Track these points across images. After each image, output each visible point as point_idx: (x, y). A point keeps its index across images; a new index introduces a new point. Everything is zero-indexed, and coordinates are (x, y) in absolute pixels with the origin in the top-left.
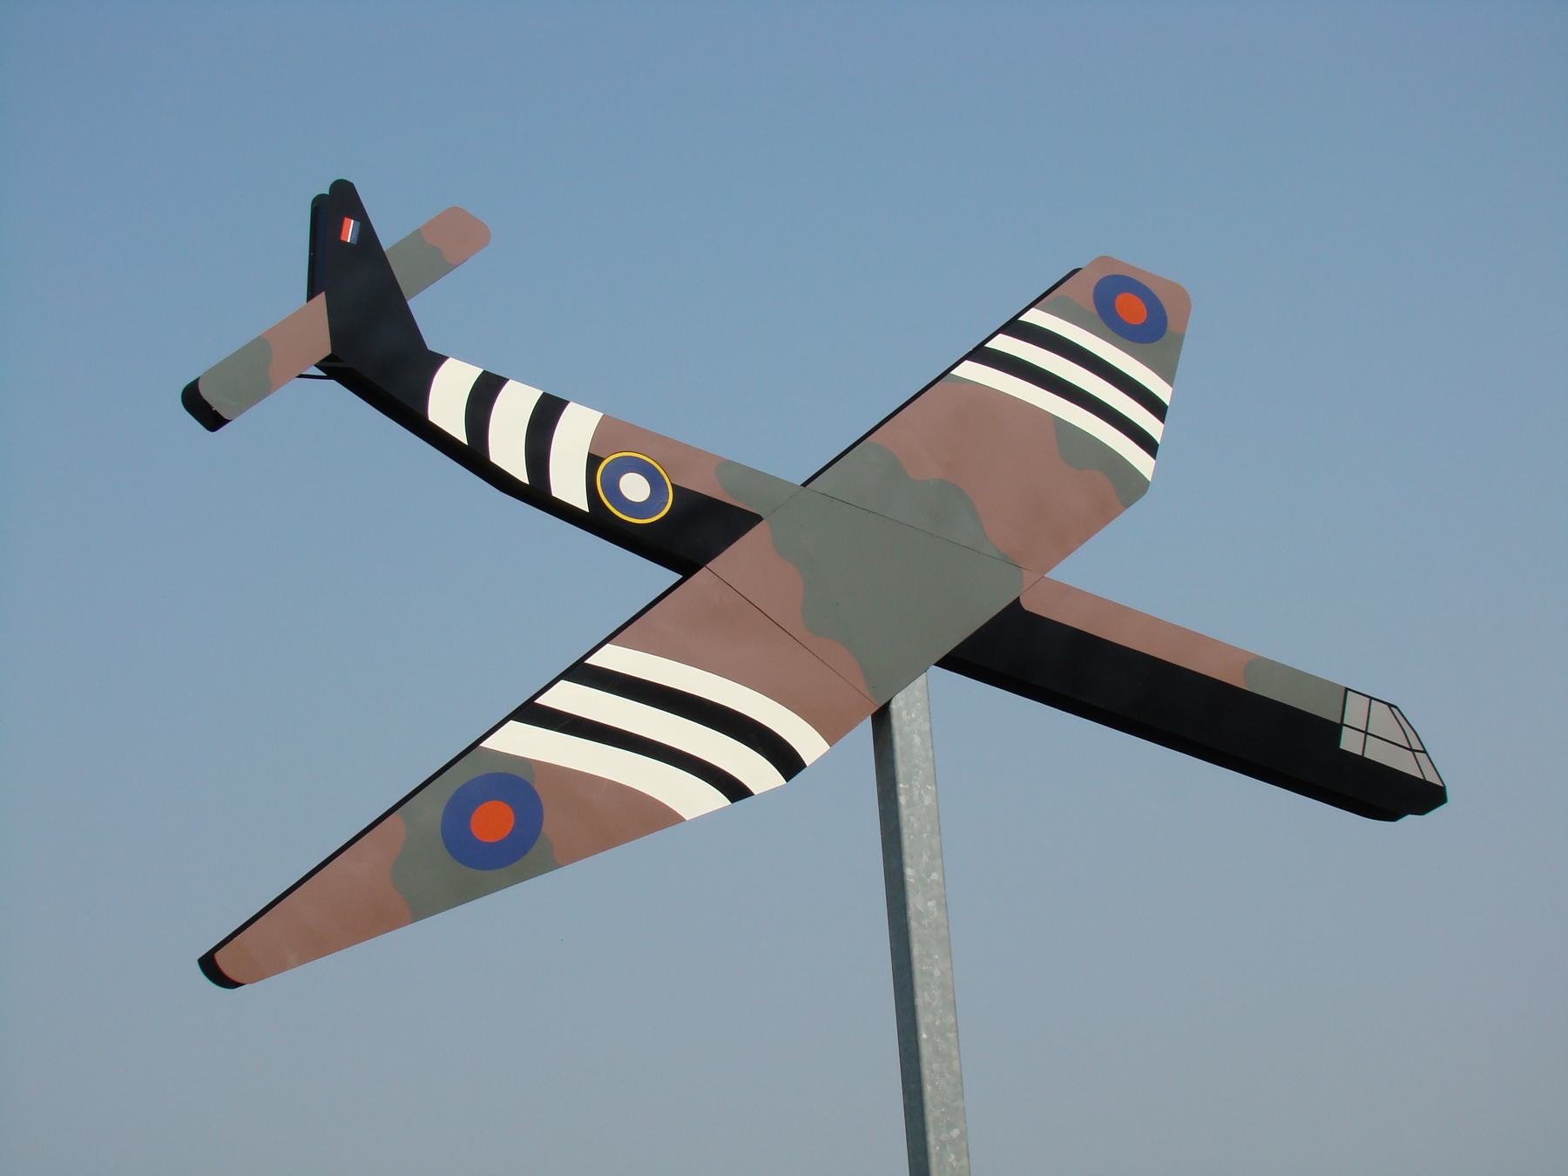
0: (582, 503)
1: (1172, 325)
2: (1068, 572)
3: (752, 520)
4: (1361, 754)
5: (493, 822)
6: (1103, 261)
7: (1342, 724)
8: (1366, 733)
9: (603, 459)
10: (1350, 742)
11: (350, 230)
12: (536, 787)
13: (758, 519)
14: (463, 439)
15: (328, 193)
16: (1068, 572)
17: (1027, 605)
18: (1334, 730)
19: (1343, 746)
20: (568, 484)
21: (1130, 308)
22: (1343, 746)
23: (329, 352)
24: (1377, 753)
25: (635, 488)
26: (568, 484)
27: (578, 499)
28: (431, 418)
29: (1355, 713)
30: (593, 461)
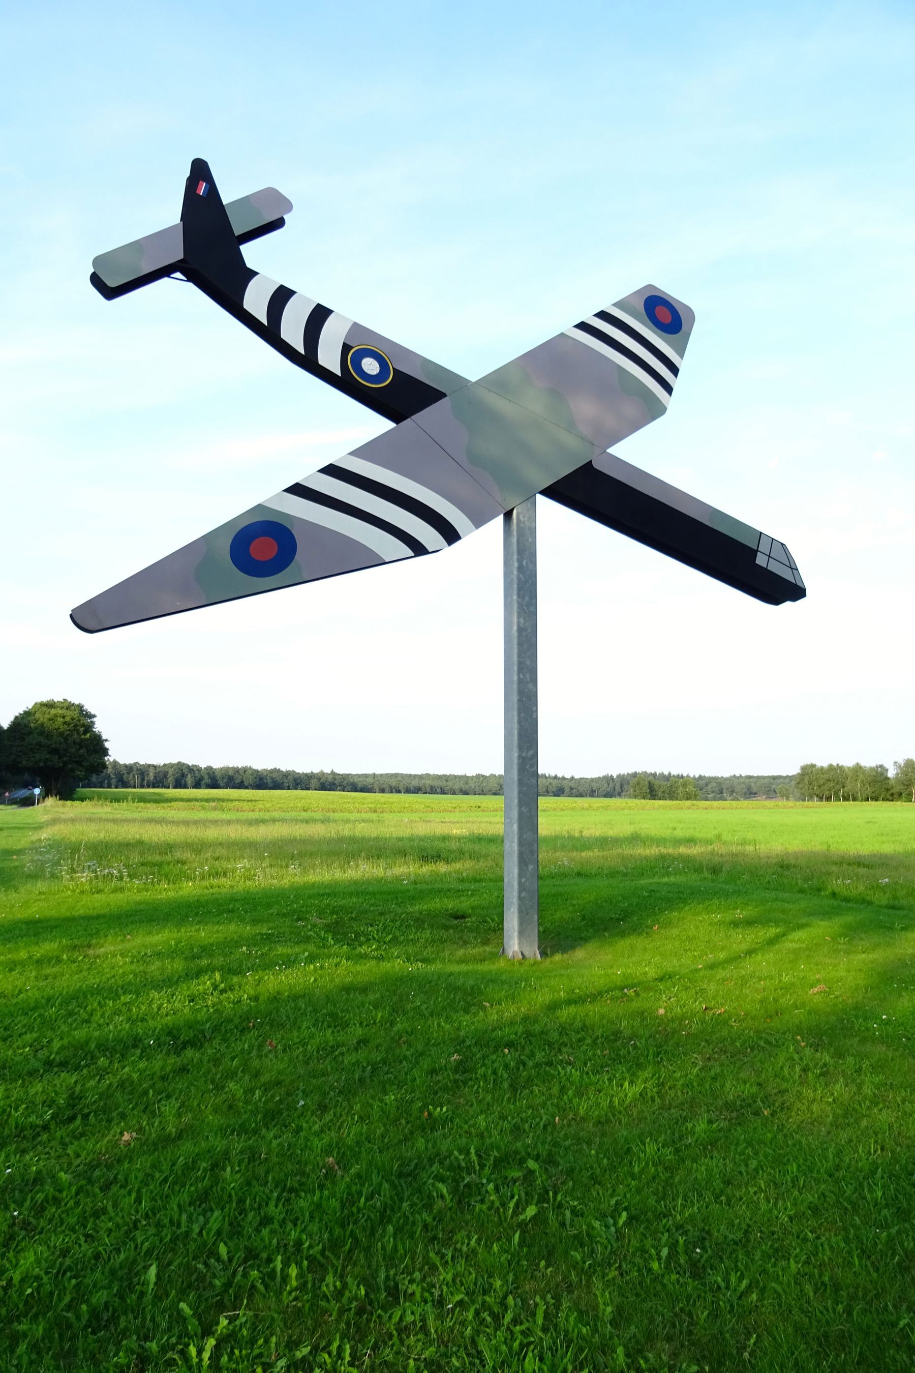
0: (337, 370)
1: (684, 327)
2: (615, 450)
3: (444, 395)
4: (237, 232)
5: (264, 549)
6: (650, 287)
7: (757, 551)
8: (769, 556)
9: (352, 348)
10: (761, 560)
11: (202, 189)
12: (294, 532)
13: (444, 395)
14: (265, 321)
15: (502, 773)
16: (615, 450)
17: (596, 465)
18: (754, 553)
19: (757, 562)
20: (329, 358)
21: (663, 314)
22: (757, 562)
23: (181, 256)
24: (774, 567)
25: (370, 366)
26: (329, 358)
27: (335, 368)
28: (245, 307)
29: (764, 547)
30: (346, 348)
